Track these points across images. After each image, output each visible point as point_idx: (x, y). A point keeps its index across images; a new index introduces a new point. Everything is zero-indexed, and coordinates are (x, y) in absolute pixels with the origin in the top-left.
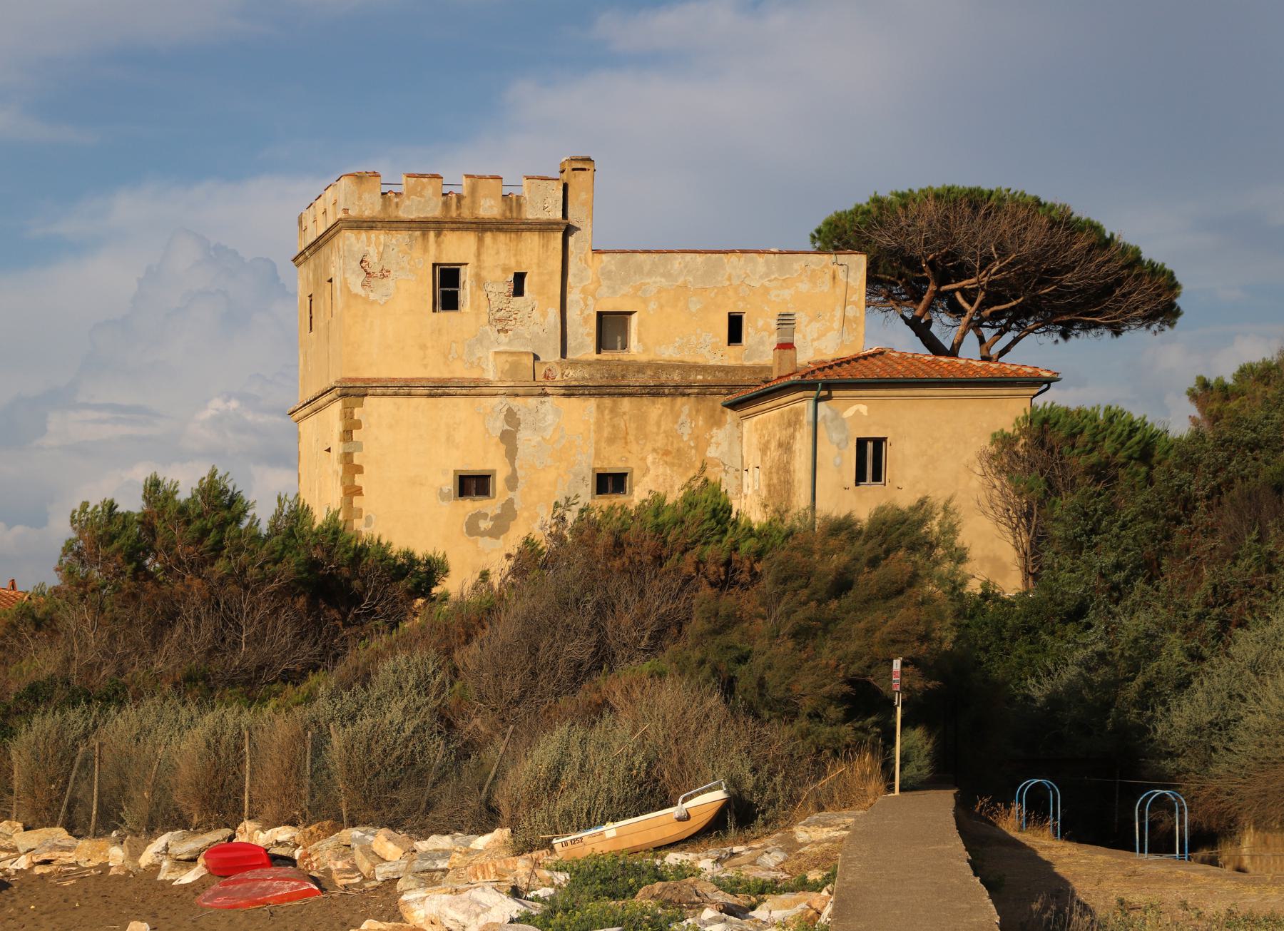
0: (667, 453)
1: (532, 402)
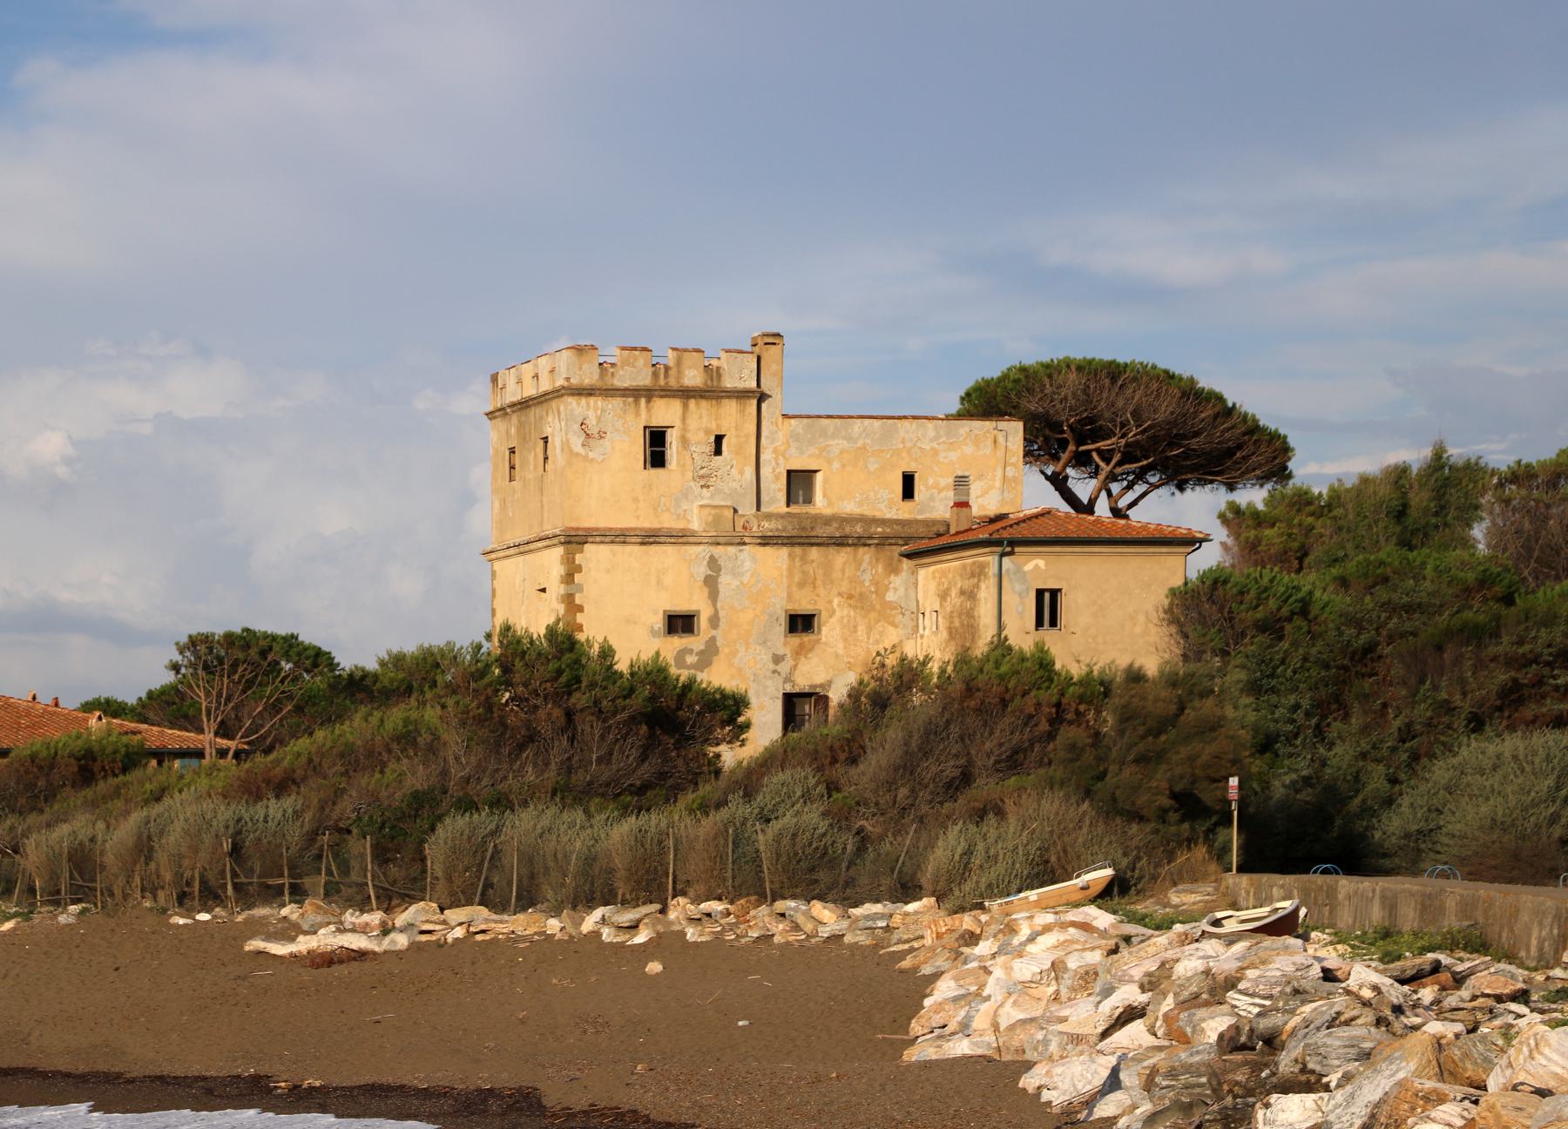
0: (850, 597)
1: (732, 550)
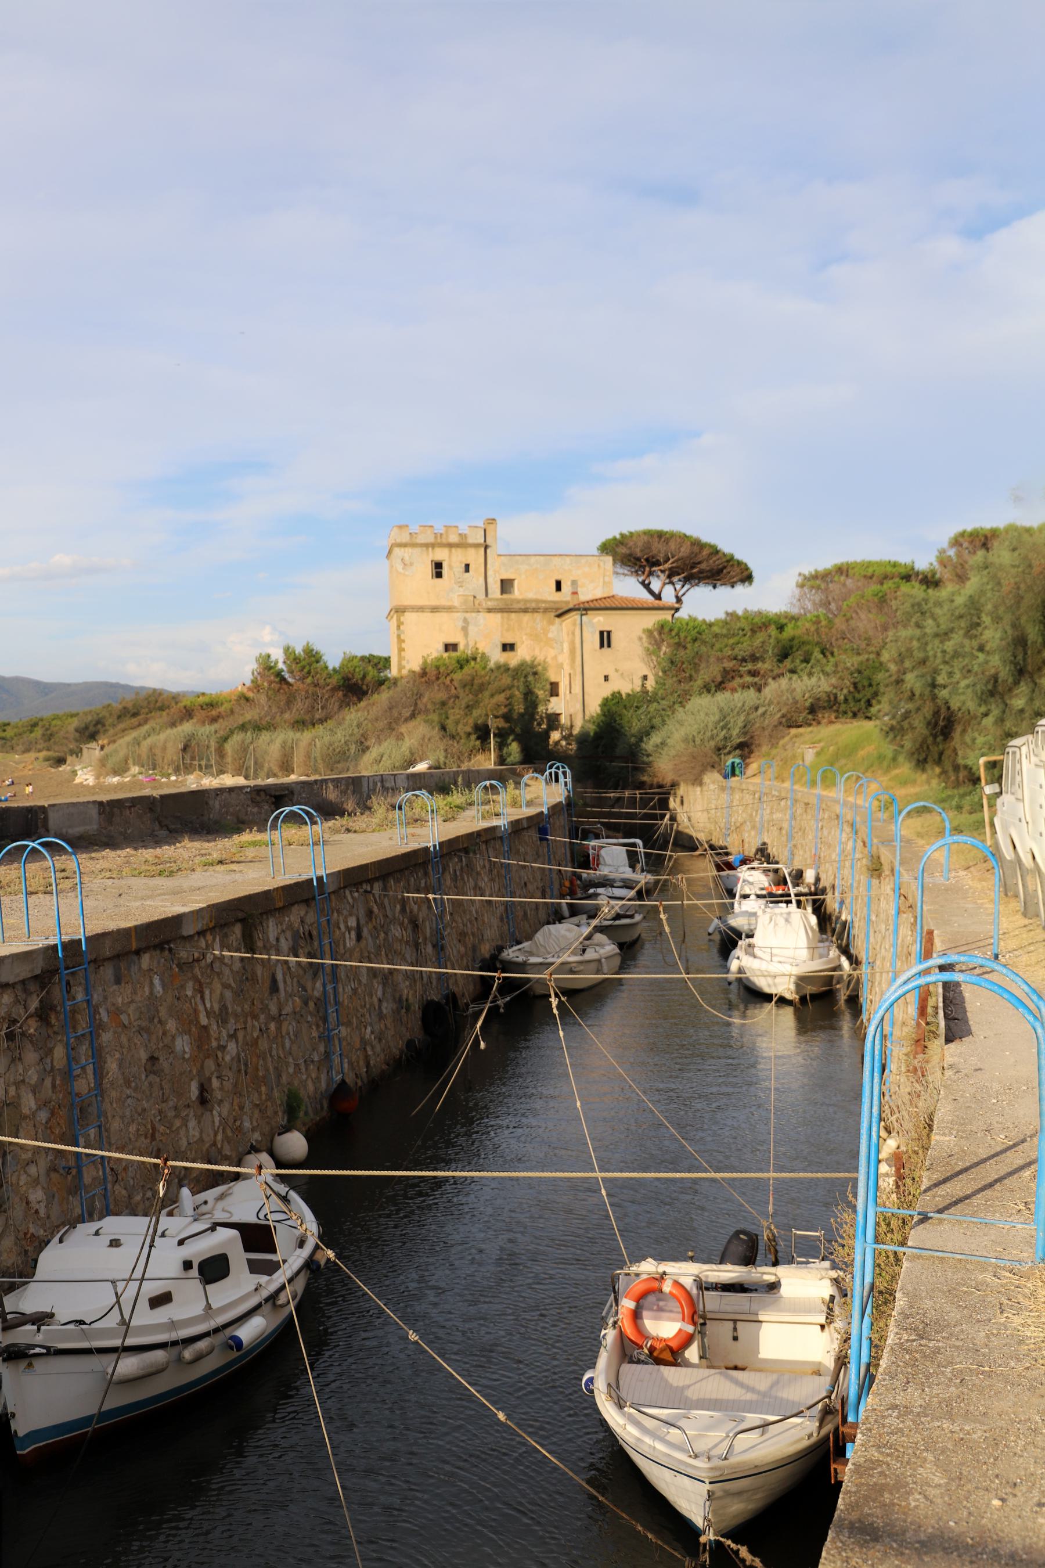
1: (474, 615)
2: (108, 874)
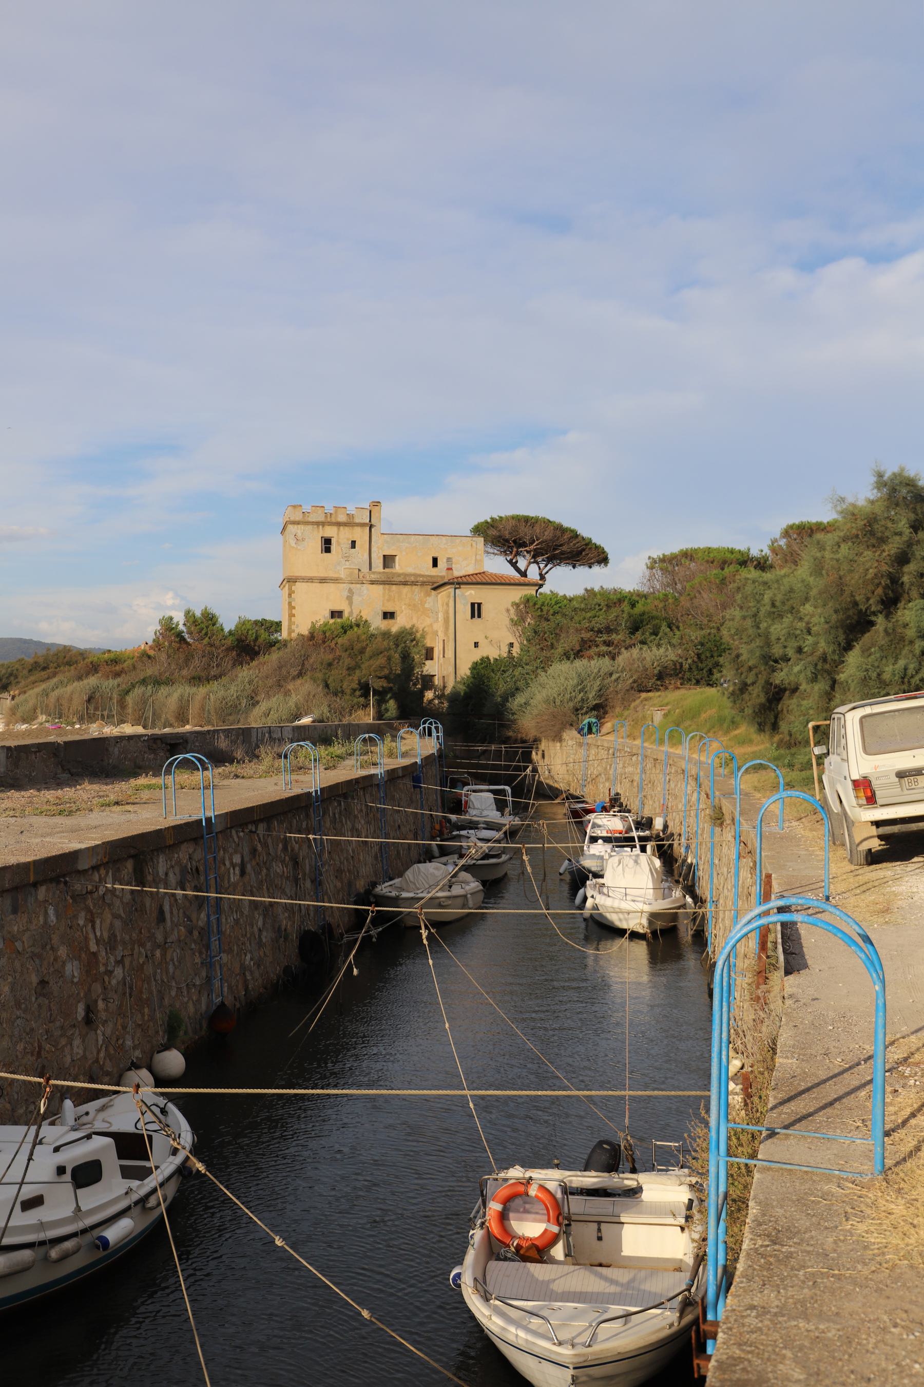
2: (12, 813)
